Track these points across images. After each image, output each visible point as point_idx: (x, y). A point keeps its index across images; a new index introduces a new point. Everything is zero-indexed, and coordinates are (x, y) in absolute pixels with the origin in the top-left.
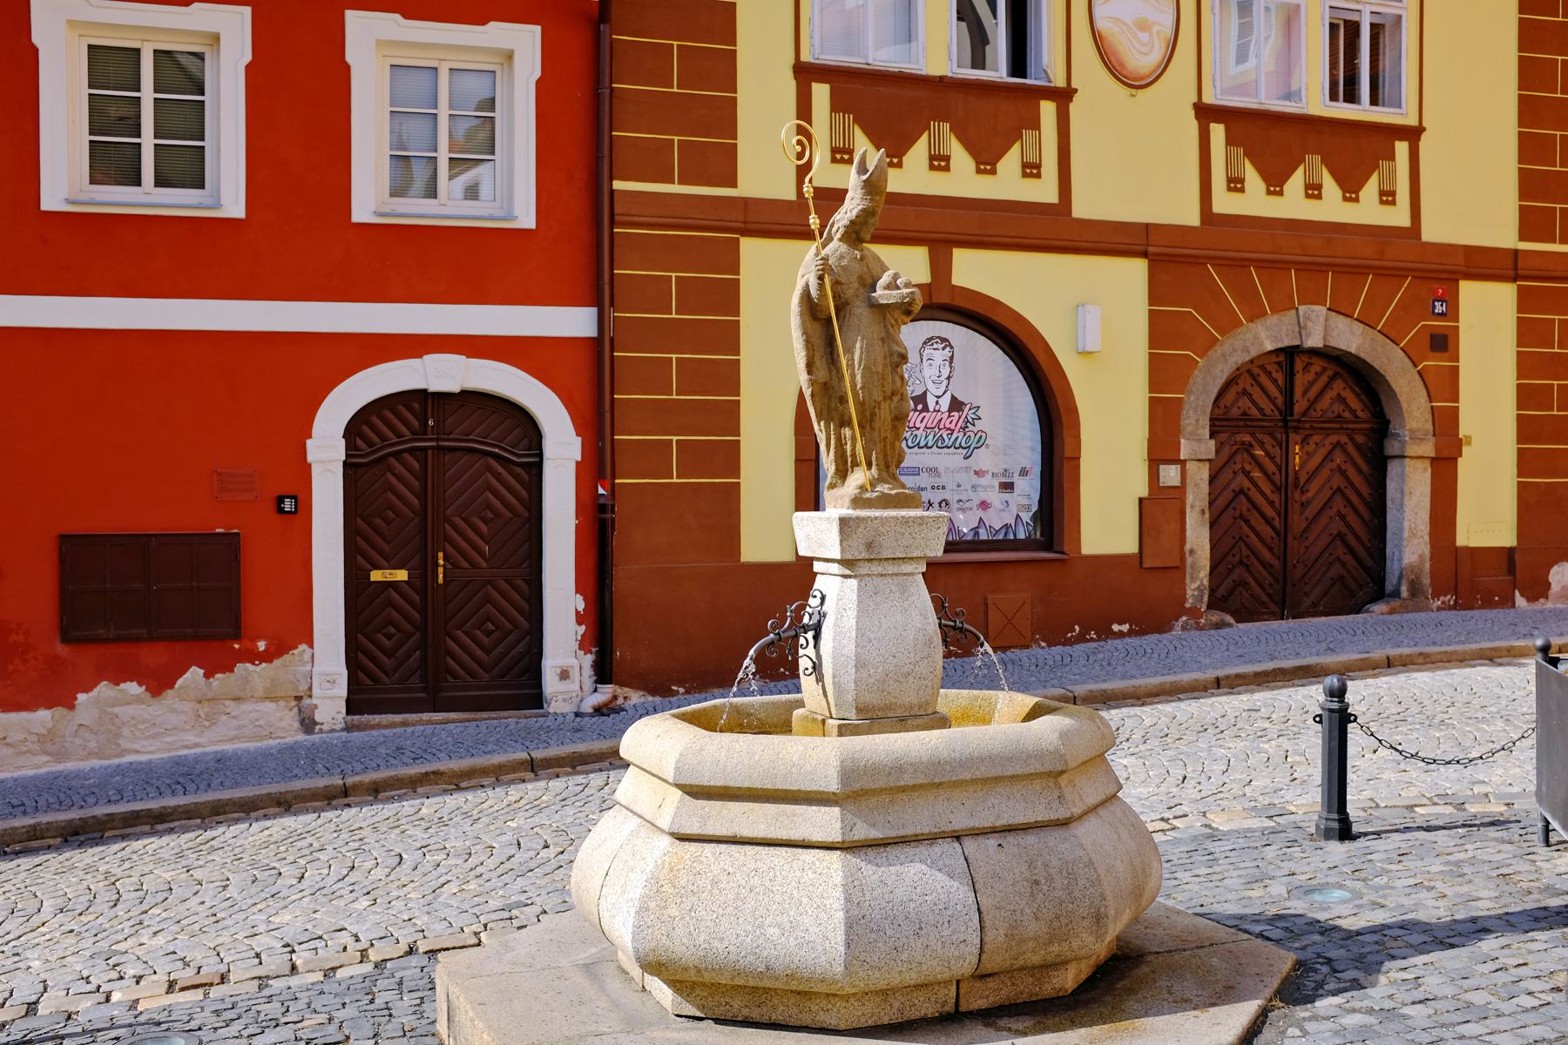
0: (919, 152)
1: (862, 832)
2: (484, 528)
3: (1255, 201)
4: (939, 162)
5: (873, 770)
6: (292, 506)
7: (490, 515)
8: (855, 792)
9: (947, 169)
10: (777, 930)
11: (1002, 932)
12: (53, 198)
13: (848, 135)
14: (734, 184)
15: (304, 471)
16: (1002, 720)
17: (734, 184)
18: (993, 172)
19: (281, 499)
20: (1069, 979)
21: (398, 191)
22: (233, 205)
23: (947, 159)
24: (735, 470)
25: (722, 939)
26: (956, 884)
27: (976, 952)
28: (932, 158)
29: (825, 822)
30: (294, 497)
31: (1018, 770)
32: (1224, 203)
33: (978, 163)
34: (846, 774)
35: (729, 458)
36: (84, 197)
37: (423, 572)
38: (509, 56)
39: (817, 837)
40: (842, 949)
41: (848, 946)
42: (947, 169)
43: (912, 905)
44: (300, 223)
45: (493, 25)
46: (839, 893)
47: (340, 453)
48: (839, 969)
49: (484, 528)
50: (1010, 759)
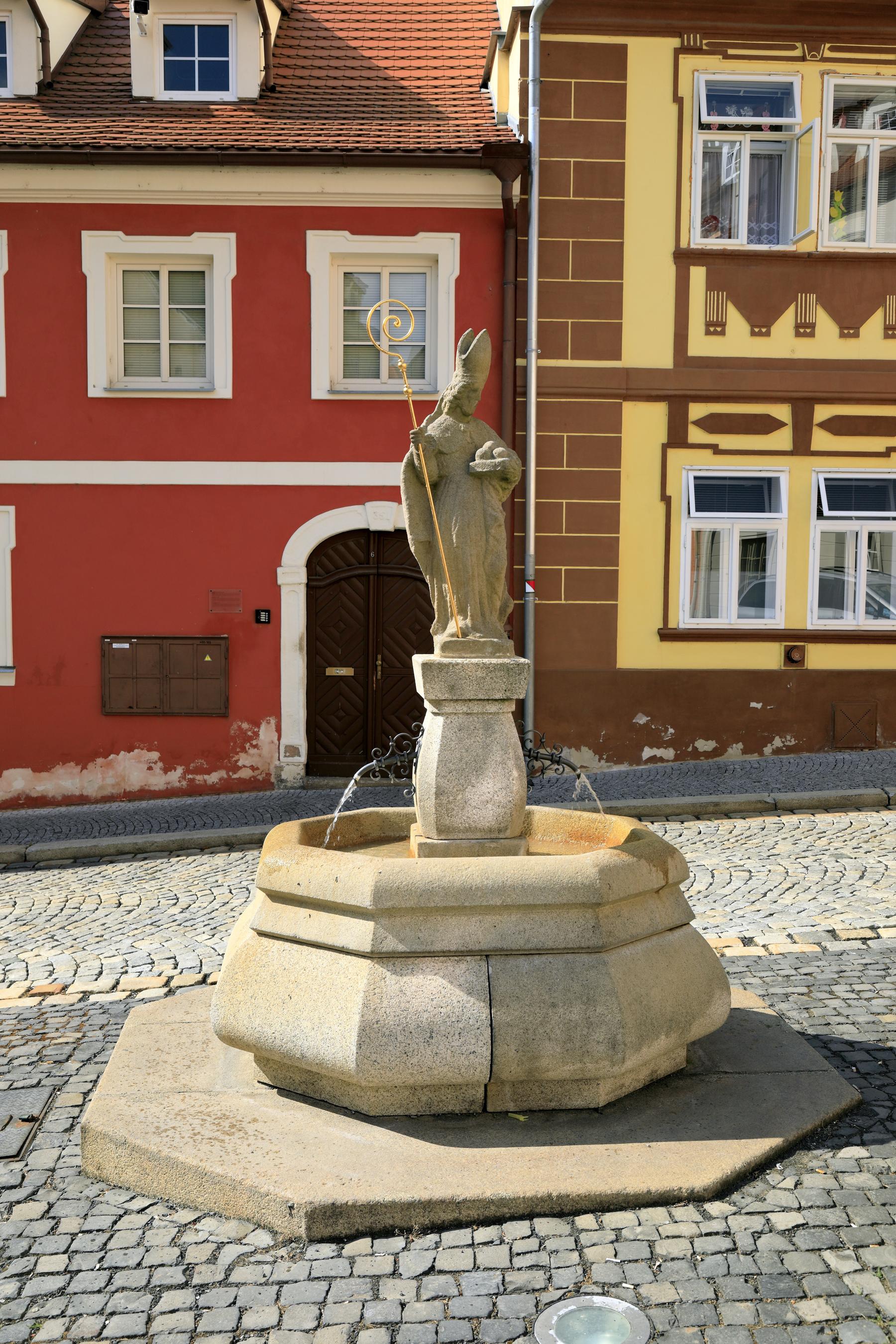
0: (786, 321)
1: (391, 944)
2: (414, 637)
3: (738, 341)
4: (805, 329)
5: (407, 891)
6: (267, 616)
7: (418, 627)
8: (386, 907)
9: (812, 335)
10: (309, 1024)
11: (513, 1047)
12: (96, 388)
13: (721, 310)
14: (618, 357)
15: (275, 591)
16: (577, 846)
17: (618, 357)
18: (856, 335)
19: (258, 613)
20: (602, 1095)
21: (349, 372)
22: (224, 389)
23: (813, 326)
24: (614, 595)
25: (271, 1025)
26: (472, 1000)
27: (487, 1063)
28: (797, 326)
29: (359, 933)
30: (268, 611)
31: (550, 900)
32: (701, 345)
33: (842, 328)
34: (379, 893)
35: (609, 585)
36: (121, 386)
37: (364, 670)
38: (435, 260)
39: (352, 946)
40: (354, 1049)
41: (359, 1046)
42: (812, 335)
43: (426, 1015)
44: (272, 401)
45: (422, 235)
46: (359, 1000)
47: (303, 577)
48: (353, 1066)
49: (414, 637)
50: (542, 890)
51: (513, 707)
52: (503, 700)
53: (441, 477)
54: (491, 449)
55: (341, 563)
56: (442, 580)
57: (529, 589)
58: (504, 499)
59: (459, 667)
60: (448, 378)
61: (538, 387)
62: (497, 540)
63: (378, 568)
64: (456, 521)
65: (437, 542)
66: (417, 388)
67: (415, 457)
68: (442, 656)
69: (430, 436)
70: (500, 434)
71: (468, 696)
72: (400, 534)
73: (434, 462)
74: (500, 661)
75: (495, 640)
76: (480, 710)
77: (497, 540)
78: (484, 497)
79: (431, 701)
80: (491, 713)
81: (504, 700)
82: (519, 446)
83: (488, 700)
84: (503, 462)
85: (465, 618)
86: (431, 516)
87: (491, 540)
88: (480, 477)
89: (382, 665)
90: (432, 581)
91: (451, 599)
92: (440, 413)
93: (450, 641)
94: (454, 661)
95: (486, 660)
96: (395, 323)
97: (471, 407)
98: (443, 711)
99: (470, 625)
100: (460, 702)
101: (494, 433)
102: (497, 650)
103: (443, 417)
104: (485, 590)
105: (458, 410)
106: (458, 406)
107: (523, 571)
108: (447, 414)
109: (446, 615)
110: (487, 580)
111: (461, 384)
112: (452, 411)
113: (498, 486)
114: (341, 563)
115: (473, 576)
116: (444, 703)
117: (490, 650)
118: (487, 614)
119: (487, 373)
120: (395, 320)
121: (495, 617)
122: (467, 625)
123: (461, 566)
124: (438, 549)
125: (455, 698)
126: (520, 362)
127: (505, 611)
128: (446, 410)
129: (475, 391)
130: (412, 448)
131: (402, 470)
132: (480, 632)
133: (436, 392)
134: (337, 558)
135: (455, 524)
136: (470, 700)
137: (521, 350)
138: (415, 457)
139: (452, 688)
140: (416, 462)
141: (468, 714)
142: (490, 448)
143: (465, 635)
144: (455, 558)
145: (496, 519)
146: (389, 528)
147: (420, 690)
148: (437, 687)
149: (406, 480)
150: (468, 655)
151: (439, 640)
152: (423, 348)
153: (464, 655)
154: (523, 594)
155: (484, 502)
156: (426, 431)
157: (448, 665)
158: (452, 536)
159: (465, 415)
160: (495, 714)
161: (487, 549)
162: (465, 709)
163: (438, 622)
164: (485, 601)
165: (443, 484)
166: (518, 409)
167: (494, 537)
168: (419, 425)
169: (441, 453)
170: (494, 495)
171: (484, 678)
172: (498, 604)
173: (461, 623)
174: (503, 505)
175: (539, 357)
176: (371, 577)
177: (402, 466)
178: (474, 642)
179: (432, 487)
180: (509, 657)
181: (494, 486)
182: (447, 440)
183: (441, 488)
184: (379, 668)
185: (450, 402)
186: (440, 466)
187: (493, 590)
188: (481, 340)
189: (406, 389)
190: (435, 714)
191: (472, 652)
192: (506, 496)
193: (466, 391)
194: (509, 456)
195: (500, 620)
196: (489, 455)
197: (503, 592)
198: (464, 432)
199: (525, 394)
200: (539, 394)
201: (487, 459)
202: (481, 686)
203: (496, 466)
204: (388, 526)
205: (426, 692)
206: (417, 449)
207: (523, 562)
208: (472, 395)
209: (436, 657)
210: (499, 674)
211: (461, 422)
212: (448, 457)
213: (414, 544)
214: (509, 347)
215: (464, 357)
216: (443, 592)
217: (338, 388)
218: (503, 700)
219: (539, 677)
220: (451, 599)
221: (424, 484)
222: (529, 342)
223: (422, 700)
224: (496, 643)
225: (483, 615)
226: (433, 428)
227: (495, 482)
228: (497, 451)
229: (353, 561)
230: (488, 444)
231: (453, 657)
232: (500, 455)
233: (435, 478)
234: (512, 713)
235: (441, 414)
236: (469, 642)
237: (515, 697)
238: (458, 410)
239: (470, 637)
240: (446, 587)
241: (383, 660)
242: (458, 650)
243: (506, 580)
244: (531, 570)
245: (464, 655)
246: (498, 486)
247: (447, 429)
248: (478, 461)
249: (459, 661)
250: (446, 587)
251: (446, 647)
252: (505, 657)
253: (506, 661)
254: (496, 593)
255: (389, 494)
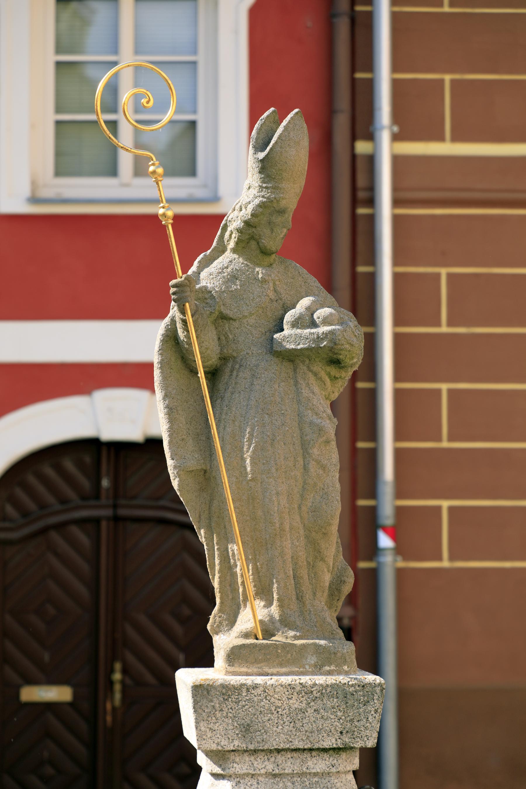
7: (186, 611)
21: (65, 164)
51: (355, 763)
52: (337, 750)
53: (224, 359)
54: (311, 311)
55: (50, 499)
56: (226, 538)
57: (385, 541)
58: (334, 396)
59: (259, 691)
60: (236, 185)
61: (395, 188)
62: (323, 468)
63: (115, 506)
64: (251, 435)
65: (218, 470)
66: (181, 193)
67: (179, 325)
68: (228, 673)
69: (205, 290)
70: (329, 286)
71: (273, 744)
72: (152, 447)
73: (211, 335)
74: (331, 680)
75: (322, 642)
76: (297, 769)
77: (323, 468)
78: (298, 393)
79: (209, 754)
80: (316, 774)
81: (339, 749)
82: (361, 303)
83: (311, 750)
84: (332, 332)
85: (269, 604)
86: (208, 426)
87: (313, 467)
88: (291, 357)
89: (123, 682)
90: (210, 540)
91: (243, 571)
92: (221, 250)
93: (243, 646)
94: (249, 680)
95: (306, 679)
96: (144, 101)
97: (274, 240)
98: (231, 771)
99: (277, 617)
100: (261, 755)
101: (314, 282)
102: (325, 661)
103: (228, 256)
104: (302, 554)
105: (253, 244)
106: (252, 238)
107: (373, 512)
108: (234, 251)
109: (235, 598)
110: (307, 537)
111: (257, 201)
112: (241, 247)
113: (323, 374)
114: (50, 499)
115: (282, 530)
116: (232, 756)
117: (312, 660)
118: (308, 596)
119: (301, 182)
120: (143, 96)
121: (320, 602)
122: (271, 617)
123: (260, 513)
124: (219, 484)
125: (251, 747)
126: (362, 147)
127: (339, 591)
128: (232, 245)
129: (282, 212)
130: (174, 310)
131: (157, 348)
132: (295, 629)
133: (215, 199)
134: (41, 489)
135: (250, 440)
136: (279, 751)
137: (363, 125)
138: (179, 325)
139: (246, 730)
140: (181, 334)
141: (275, 776)
142: (308, 308)
143: (268, 633)
144: (249, 500)
145: (321, 430)
146: (135, 434)
147: (190, 732)
148: (219, 727)
149: (162, 351)
150: (275, 670)
151: (222, 643)
152: (193, 124)
153: (266, 670)
154: (374, 551)
155: (299, 402)
156: (198, 281)
157: (238, 689)
158: (243, 460)
159: (265, 252)
160: (323, 775)
161: (305, 483)
162: (270, 767)
163: (220, 611)
164: (304, 573)
165: (227, 370)
166: (361, 226)
167: (318, 462)
168: (185, 270)
169: (223, 317)
170: (316, 389)
171: (303, 711)
172: (327, 578)
173: (262, 613)
174: (333, 405)
175: (396, 138)
176: (104, 524)
177: (158, 329)
178: (285, 646)
179: (204, 375)
180: (347, 673)
181: (316, 374)
182: (235, 296)
183: (225, 378)
184: (118, 687)
185: (239, 231)
186: (222, 339)
187: (318, 554)
188: (292, 127)
189: (162, 196)
190: (216, 776)
191: (281, 665)
192: (338, 389)
193: (266, 212)
194: (341, 322)
195: (330, 608)
196: (307, 321)
197: (336, 556)
198: (264, 281)
199: (371, 201)
200: (396, 202)
201: (304, 327)
202: (299, 724)
203: (319, 339)
204: (133, 432)
205: (200, 737)
206: (183, 312)
207: (373, 493)
208: (278, 219)
209: (217, 673)
210: (329, 704)
211: (259, 265)
212: (236, 324)
213: (179, 475)
214: (342, 123)
215: (261, 155)
216: (228, 557)
217: (45, 193)
218: (337, 750)
219: (406, 698)
220: (243, 571)
221: (194, 372)
222: (377, 113)
223: (193, 752)
224: (324, 648)
225: (300, 598)
226: (211, 274)
227: (319, 367)
228: (321, 313)
229: (70, 493)
230: (305, 302)
231: (247, 674)
232: (326, 321)
233: (214, 361)
234: (354, 772)
235: (223, 251)
236: (275, 646)
237: (359, 744)
238: (253, 244)
239: (279, 638)
240: (235, 548)
241: (125, 671)
242: (256, 661)
243: (341, 536)
244: (387, 506)
245: (266, 670)
246: (323, 374)
247: (233, 277)
248: (287, 331)
249: (259, 680)
250: (235, 548)
251: (235, 655)
252: (339, 673)
253: (342, 679)
254: (322, 560)
255: (133, 375)
